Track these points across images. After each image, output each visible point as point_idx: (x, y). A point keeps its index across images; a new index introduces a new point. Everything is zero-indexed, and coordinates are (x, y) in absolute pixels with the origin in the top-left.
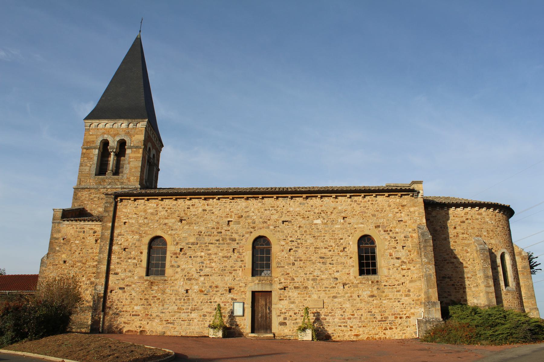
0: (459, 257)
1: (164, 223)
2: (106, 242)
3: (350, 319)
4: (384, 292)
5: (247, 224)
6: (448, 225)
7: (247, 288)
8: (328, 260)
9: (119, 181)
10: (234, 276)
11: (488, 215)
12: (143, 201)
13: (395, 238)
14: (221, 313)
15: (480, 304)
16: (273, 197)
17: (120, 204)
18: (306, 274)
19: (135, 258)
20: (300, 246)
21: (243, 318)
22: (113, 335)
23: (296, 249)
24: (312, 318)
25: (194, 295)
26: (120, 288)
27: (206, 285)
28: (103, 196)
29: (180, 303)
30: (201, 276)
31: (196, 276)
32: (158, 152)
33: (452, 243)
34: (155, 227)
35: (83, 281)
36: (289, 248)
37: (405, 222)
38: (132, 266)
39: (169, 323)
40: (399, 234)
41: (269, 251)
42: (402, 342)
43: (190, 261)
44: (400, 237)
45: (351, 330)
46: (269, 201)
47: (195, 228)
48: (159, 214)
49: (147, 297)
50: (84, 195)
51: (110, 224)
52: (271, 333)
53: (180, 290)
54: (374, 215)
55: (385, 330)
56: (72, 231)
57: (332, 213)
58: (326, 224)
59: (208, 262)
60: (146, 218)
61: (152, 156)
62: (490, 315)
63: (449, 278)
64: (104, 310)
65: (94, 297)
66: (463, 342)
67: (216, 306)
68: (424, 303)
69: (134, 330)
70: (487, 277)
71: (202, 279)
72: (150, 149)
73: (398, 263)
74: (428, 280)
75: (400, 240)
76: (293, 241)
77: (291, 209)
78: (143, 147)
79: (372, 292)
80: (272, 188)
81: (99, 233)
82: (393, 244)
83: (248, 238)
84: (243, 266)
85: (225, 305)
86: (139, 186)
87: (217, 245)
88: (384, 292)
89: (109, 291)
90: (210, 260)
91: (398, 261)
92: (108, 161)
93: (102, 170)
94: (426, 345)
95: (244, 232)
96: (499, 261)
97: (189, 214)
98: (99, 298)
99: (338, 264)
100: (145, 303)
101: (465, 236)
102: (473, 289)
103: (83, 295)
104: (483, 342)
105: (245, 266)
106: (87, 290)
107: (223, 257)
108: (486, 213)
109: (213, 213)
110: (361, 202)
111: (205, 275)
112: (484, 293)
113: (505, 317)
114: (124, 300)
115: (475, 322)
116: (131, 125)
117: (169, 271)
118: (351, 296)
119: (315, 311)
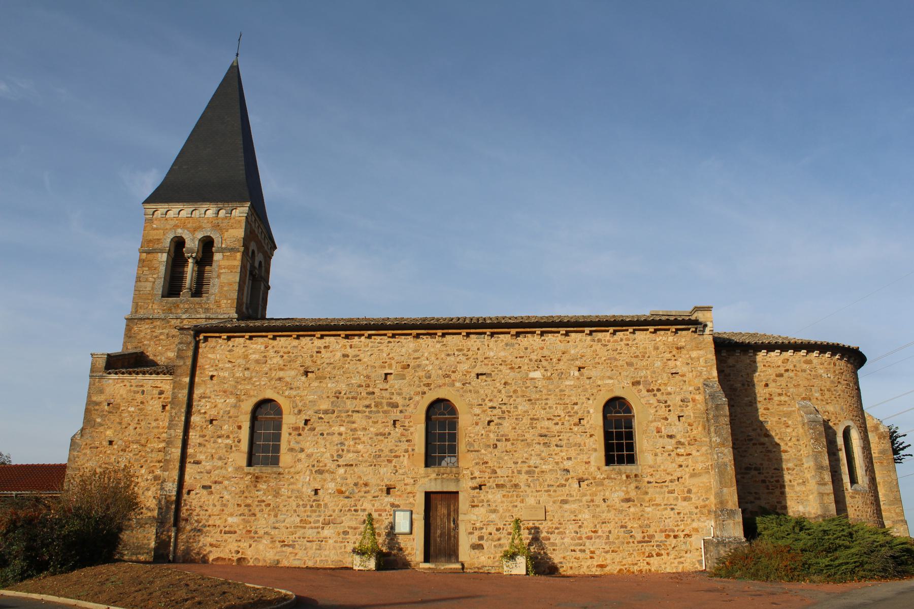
0: (773, 434)
1: (277, 377)
2: (180, 409)
3: (589, 538)
4: (647, 493)
5: (416, 379)
6: (755, 380)
7: (417, 486)
8: (554, 439)
9: (202, 307)
10: (395, 467)
11: (822, 364)
12: (242, 340)
13: (666, 402)
14: (373, 529)
15: (809, 513)
16: (460, 334)
17: (203, 345)
18: (516, 463)
19: (228, 437)
20: (506, 415)
21: (411, 537)
22: (192, 565)
23: (500, 421)
24: (526, 536)
25: (327, 499)
26: (204, 487)
27: (349, 481)
28: (175, 332)
29: (305, 511)
30: (339, 466)
31: (331, 466)
32: (268, 257)
33: (761, 411)
34: (263, 383)
35: (142, 475)
36: (488, 419)
37: (683, 376)
38: (224, 450)
39: (285, 545)
40: (673, 396)
41: (453, 425)
42: (678, 577)
43: (321, 442)
44: (675, 400)
45: (591, 558)
46: (454, 341)
47: (329, 385)
48: (269, 362)
49: (249, 501)
50: (144, 329)
51: (187, 380)
52: (458, 561)
53: (304, 490)
54: (630, 364)
55: (649, 556)
56: (123, 392)
57: (559, 360)
58: (549, 378)
59: (352, 443)
60: (248, 369)
61: (257, 264)
62: (825, 532)
63: (756, 469)
64: (176, 523)
65: (160, 501)
66: (781, 578)
67: (365, 517)
68: (715, 512)
69: (226, 557)
70: (820, 468)
71: (341, 471)
72: (253, 252)
73: (670, 444)
74: (721, 474)
75: (675, 405)
76: (495, 408)
77: (492, 354)
78: (242, 249)
79: (627, 493)
80: (459, 319)
81: (168, 394)
82: (663, 412)
83: (418, 402)
84: (410, 449)
85: (380, 515)
86: (236, 316)
87: (367, 414)
88: (647, 493)
89: (185, 491)
90: (354, 439)
91: (670, 440)
92: (183, 272)
93: (173, 288)
94: (717, 583)
95: (412, 393)
96: (840, 441)
97: (319, 362)
98: (168, 502)
99: (569, 445)
100: (246, 511)
101: (783, 398)
102: (798, 488)
103: (141, 498)
104: (815, 578)
105: (413, 450)
106: (148, 489)
107: (377, 435)
108: (819, 361)
109: (360, 360)
110: (609, 341)
111: (346, 465)
112: (815, 494)
113: (851, 534)
114: (211, 507)
115: (801, 545)
116: (222, 213)
117: (285, 458)
118: (592, 501)
119: (531, 525)
